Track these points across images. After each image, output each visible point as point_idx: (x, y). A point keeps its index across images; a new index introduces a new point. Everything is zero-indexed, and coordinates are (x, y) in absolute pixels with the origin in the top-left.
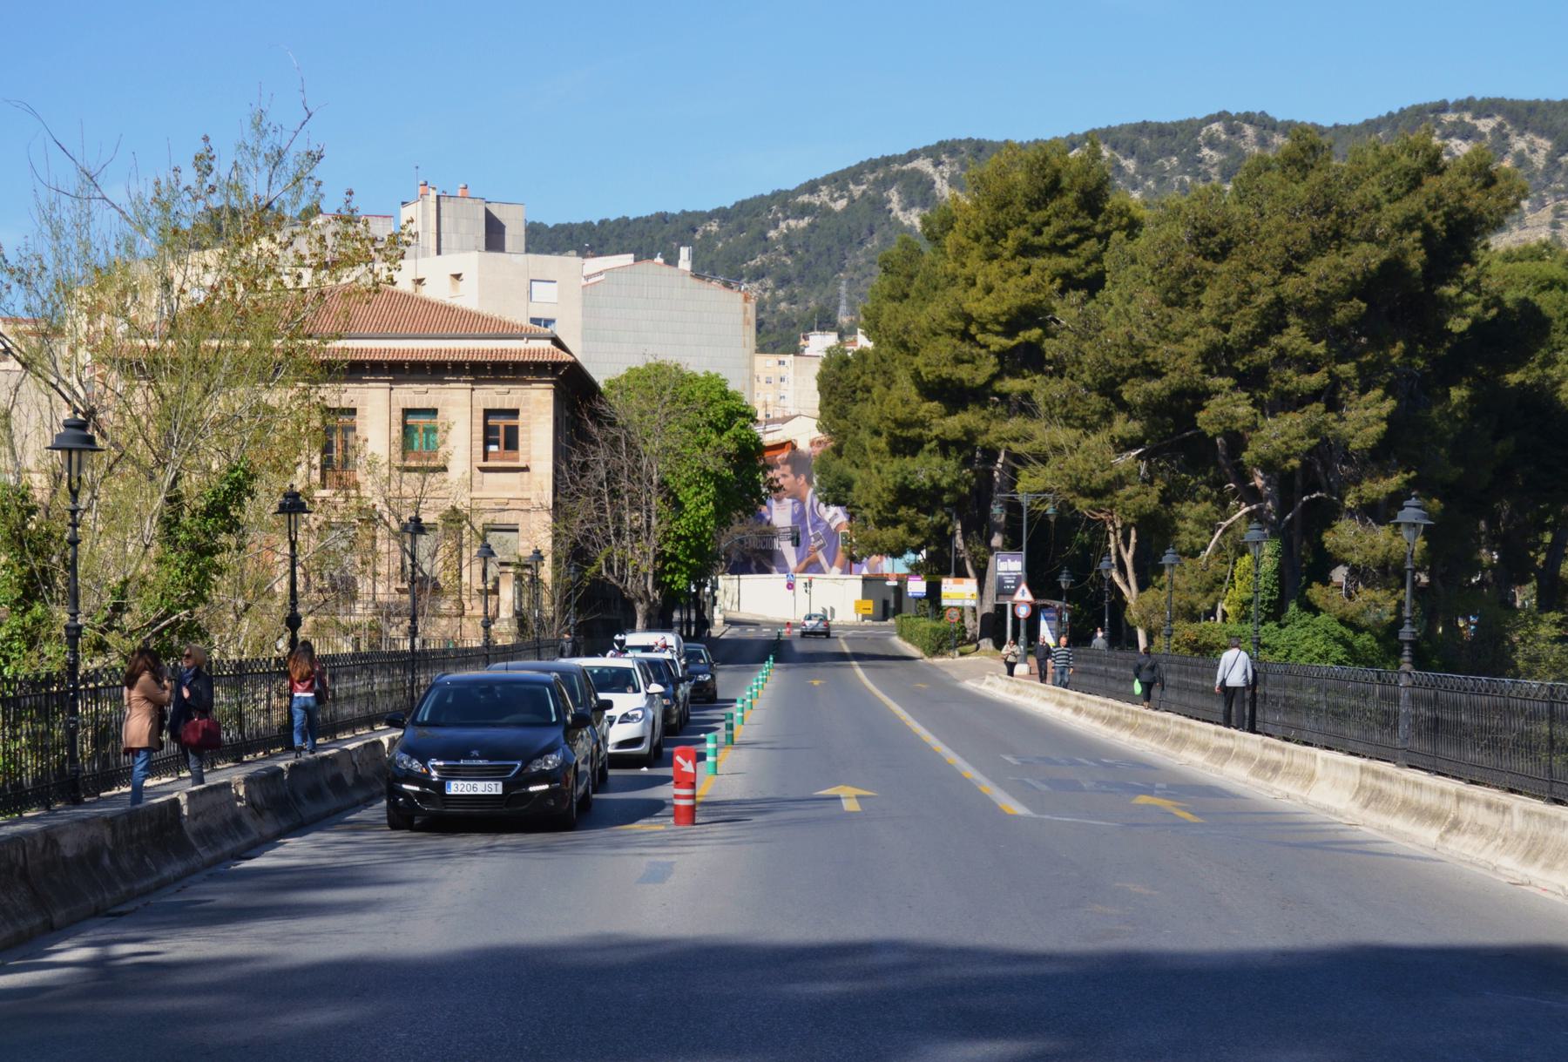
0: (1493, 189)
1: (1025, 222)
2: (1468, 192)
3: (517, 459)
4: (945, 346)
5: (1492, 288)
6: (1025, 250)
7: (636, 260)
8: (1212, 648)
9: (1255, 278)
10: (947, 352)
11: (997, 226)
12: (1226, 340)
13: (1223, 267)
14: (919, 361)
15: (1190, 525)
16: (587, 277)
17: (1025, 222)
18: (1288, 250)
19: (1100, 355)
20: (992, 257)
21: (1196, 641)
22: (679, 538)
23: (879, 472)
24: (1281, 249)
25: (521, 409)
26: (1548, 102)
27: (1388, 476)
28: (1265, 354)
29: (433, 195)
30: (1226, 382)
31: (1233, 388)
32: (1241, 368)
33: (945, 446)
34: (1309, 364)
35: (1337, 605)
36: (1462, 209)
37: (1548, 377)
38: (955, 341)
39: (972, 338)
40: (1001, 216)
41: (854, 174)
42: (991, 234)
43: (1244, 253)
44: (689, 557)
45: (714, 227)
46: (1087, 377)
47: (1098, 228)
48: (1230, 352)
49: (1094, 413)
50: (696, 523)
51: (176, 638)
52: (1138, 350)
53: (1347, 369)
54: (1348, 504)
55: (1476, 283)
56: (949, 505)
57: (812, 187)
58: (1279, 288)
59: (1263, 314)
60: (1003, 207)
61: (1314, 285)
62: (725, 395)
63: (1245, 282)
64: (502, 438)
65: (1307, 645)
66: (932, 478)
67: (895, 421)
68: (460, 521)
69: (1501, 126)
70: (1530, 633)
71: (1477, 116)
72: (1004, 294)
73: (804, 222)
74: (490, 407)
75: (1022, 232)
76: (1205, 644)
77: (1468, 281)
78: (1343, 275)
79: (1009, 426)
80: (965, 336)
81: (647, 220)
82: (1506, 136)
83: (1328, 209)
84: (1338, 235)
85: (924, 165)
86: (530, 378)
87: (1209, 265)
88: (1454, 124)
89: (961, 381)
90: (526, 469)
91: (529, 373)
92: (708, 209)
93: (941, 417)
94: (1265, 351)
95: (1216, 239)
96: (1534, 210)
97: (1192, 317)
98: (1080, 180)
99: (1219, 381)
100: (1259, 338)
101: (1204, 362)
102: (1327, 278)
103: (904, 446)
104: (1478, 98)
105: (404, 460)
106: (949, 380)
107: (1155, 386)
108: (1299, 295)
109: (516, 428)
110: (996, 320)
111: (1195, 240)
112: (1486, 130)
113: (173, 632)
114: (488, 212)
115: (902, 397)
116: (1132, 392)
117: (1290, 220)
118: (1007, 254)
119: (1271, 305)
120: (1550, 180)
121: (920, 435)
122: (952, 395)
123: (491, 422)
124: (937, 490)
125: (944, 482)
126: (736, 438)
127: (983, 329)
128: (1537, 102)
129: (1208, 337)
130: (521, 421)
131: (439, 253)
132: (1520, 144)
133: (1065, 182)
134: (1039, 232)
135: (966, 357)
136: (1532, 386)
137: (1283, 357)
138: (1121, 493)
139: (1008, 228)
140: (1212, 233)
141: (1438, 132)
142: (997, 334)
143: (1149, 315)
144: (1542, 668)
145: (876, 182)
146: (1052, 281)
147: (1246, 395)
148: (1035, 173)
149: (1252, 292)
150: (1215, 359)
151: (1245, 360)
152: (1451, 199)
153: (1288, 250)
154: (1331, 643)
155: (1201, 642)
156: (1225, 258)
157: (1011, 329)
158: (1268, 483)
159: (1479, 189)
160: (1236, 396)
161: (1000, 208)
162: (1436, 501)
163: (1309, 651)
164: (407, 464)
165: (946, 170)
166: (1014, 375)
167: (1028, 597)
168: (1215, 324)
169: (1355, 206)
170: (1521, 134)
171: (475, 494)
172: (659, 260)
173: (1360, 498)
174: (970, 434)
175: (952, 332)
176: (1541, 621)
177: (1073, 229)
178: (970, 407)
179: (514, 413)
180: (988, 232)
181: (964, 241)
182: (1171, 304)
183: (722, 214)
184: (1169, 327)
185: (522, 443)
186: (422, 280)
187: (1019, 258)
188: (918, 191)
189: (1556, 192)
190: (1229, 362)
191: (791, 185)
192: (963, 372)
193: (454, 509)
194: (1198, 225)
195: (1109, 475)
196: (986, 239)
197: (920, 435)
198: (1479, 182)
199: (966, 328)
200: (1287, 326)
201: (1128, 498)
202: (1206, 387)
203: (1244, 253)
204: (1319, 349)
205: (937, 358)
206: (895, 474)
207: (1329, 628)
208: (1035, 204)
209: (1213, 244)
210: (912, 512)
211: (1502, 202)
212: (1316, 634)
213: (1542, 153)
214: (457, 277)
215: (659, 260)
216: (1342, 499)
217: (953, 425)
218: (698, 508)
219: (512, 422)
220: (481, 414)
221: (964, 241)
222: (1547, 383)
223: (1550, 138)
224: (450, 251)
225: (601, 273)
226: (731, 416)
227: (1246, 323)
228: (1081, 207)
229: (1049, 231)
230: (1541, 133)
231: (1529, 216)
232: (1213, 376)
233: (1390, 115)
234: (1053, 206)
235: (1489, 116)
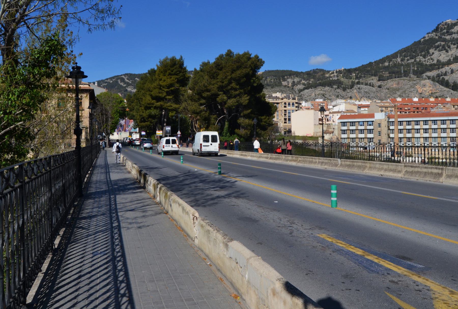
4: (157, 90)
6: (170, 74)
10: (157, 91)
14: (152, 93)
15: (213, 119)
27: (248, 110)
28: (229, 87)
30: (222, 93)
31: (223, 94)
33: (156, 108)
34: (236, 90)
40: (166, 68)
41: (113, 77)
47: (182, 71)
51: (13, 140)
52: (206, 87)
53: (242, 91)
56: (157, 118)
57: (107, 79)
73: (106, 84)
75: (169, 71)
80: (160, 89)
85: (123, 77)
87: (219, 71)
89: (160, 96)
99: (220, 93)
103: (147, 108)
107: (209, 93)
110: (166, 86)
111: (216, 67)
113: (11, 137)
115: (148, 99)
116: (205, 94)
122: (158, 99)
124: (156, 115)
125: (157, 114)
127: (164, 87)
134: (172, 71)
137: (232, 88)
138: (202, 113)
140: (219, 66)
142: (166, 88)
145: (116, 79)
150: (221, 88)
157: (168, 88)
161: (165, 67)
165: (126, 77)
166: (169, 96)
167: (180, 133)
168: (221, 82)
174: (161, 105)
177: (178, 71)
182: (211, 78)
188: (123, 80)
191: (104, 79)
192: (160, 95)
195: (200, 110)
196: (163, 72)
199: (160, 87)
200: (232, 83)
201: (203, 114)
204: (238, 87)
205: (155, 92)
229: (174, 71)
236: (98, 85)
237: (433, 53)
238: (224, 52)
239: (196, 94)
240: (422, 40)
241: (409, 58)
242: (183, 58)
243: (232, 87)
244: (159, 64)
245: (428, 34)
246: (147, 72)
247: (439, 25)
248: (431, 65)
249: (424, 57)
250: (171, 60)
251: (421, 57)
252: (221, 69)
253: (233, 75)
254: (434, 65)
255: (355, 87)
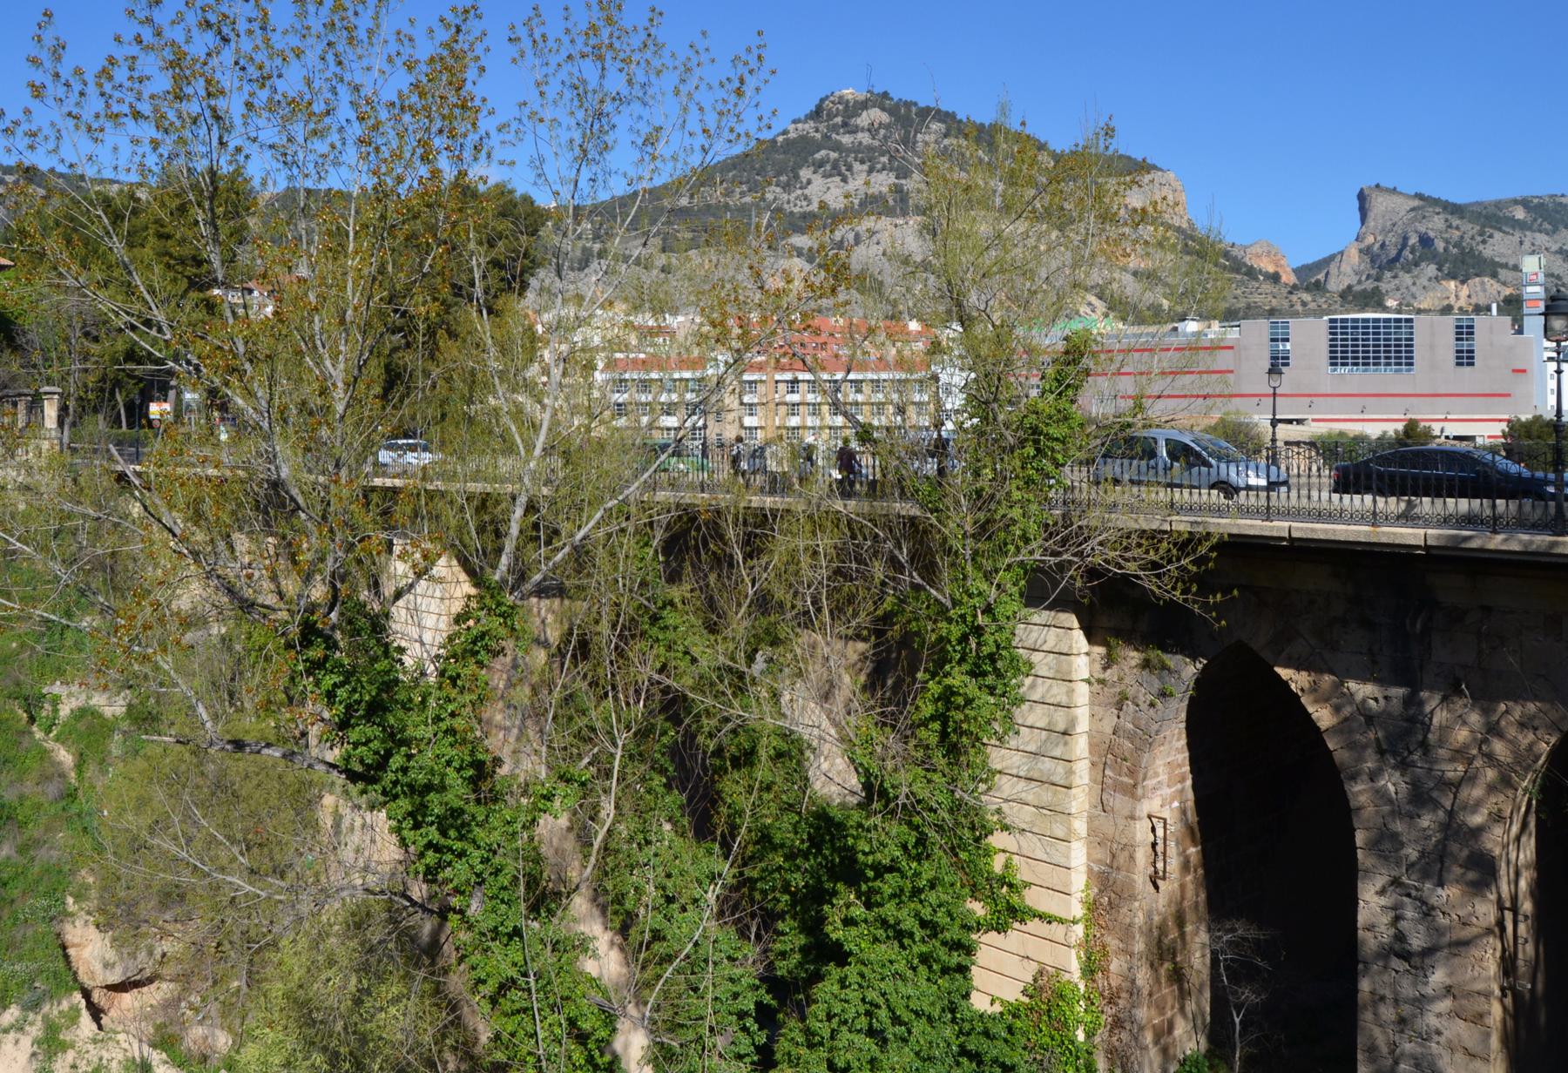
237: (809, 182)
240: (780, 139)
241: (744, 188)
245: (795, 122)
247: (822, 101)
248: (804, 216)
249: (787, 187)
251: (778, 190)
254: (813, 215)
255: (594, 265)
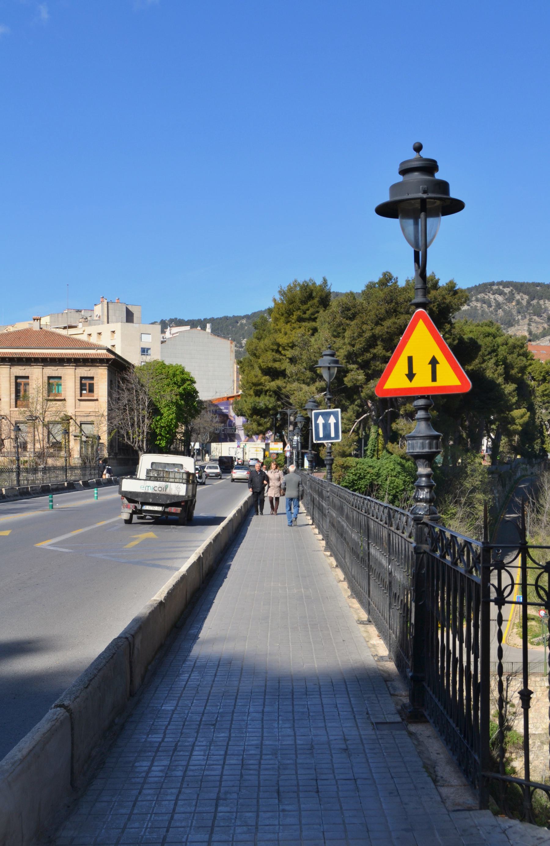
0: (457, 296)
1: (299, 309)
2: (446, 296)
3: (93, 396)
4: (270, 355)
5: (456, 333)
6: (300, 320)
7: (191, 328)
8: (350, 467)
9: (365, 327)
10: (270, 357)
11: (290, 310)
12: (354, 350)
13: (352, 323)
14: (260, 361)
16: (173, 334)
17: (299, 309)
18: (377, 316)
19: (308, 356)
20: (288, 322)
21: (343, 465)
22: (162, 427)
23: (246, 402)
24: (374, 316)
25: (95, 376)
26: (527, 283)
28: (368, 356)
29: (106, 302)
30: (354, 366)
31: (358, 369)
32: (360, 361)
35: (396, 450)
36: (444, 303)
37: (481, 367)
38: (274, 353)
39: (280, 352)
40: (291, 307)
42: (288, 313)
43: (361, 317)
44: (167, 434)
45: (244, 321)
46: (304, 364)
48: (356, 355)
49: (308, 378)
50: (168, 421)
54: (401, 412)
55: (450, 331)
56: (272, 415)
58: (373, 331)
59: (367, 341)
60: (292, 303)
61: (386, 330)
62: (183, 372)
63: (361, 328)
64: (87, 388)
65: (387, 466)
66: (265, 404)
67: (253, 383)
68: (68, 420)
69: (512, 290)
70: (472, 461)
71: (504, 287)
72: (291, 336)
74: (82, 376)
75: (299, 313)
76: (347, 466)
77: (447, 330)
78: (397, 326)
79: (294, 385)
80: (278, 351)
81: (221, 319)
82: (513, 294)
83: (392, 301)
84: (395, 311)
86: (98, 365)
87: (348, 322)
88: (497, 289)
89: (276, 368)
90: (97, 400)
91: (97, 363)
92: (242, 315)
93: (269, 382)
94: (368, 355)
95: (351, 312)
96: (522, 319)
97: (342, 342)
98: (320, 294)
100: (366, 350)
101: (347, 359)
102: (390, 327)
104: (505, 281)
105: (49, 396)
106: (271, 368)
108: (380, 333)
109: (93, 384)
111: (343, 312)
112: (507, 292)
114: (127, 308)
117: (378, 305)
118: (293, 321)
119: (370, 337)
120: (528, 309)
121: (262, 389)
123: (83, 381)
125: (270, 406)
126: (184, 389)
127: (284, 349)
128: (524, 283)
129: (347, 349)
130: (95, 381)
131: (108, 323)
132: (518, 297)
133: (314, 294)
134: (305, 313)
135: (277, 359)
136: (476, 371)
137: (375, 357)
139: (294, 311)
141: (491, 292)
143: (327, 341)
144: (476, 474)
146: (309, 331)
147: (362, 371)
148: (303, 291)
149: (363, 332)
150: (350, 357)
151: (361, 358)
152: (440, 299)
153: (377, 316)
154: (396, 465)
155: (345, 465)
156: (354, 319)
158: (373, 405)
159: (451, 296)
160: (358, 372)
161: (290, 304)
162: (435, 412)
163: (387, 468)
164: (50, 398)
168: (349, 344)
169: (402, 300)
170: (518, 294)
171: (76, 410)
172: (199, 328)
173: (406, 410)
175: (273, 350)
176: (476, 456)
178: (280, 378)
179: (92, 378)
180: (286, 313)
181: (278, 316)
182: (335, 337)
183: (247, 317)
184: (334, 345)
185: (95, 390)
186: (162, 343)
187: (297, 323)
189: (530, 313)
190: (356, 359)
193: (66, 416)
194: (344, 306)
196: (286, 315)
197: (262, 389)
198: (451, 293)
200: (377, 345)
202: (347, 368)
203: (361, 317)
206: (251, 403)
207: (396, 459)
208: (304, 302)
209: (350, 313)
210: (258, 417)
211: (460, 301)
212: (390, 462)
213: (526, 300)
214: (113, 332)
215: (199, 328)
216: (399, 410)
217: (273, 385)
218: (168, 416)
219: (91, 382)
220: (79, 379)
221: (278, 316)
222: (482, 369)
223: (528, 295)
224: (113, 322)
225: (177, 333)
226: (184, 381)
227: (361, 344)
228: (320, 304)
229: (308, 313)
230: (525, 294)
231: (521, 321)
232: (350, 364)
233: (476, 286)
234: (310, 303)
235: (508, 287)
236: (212, 330)
238: (376, 278)
239: (306, 369)
242: (329, 283)
243: (375, 355)
244: (278, 297)
246: (360, 292)
250: (301, 288)
252: (352, 318)
253: (378, 330)
